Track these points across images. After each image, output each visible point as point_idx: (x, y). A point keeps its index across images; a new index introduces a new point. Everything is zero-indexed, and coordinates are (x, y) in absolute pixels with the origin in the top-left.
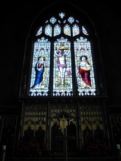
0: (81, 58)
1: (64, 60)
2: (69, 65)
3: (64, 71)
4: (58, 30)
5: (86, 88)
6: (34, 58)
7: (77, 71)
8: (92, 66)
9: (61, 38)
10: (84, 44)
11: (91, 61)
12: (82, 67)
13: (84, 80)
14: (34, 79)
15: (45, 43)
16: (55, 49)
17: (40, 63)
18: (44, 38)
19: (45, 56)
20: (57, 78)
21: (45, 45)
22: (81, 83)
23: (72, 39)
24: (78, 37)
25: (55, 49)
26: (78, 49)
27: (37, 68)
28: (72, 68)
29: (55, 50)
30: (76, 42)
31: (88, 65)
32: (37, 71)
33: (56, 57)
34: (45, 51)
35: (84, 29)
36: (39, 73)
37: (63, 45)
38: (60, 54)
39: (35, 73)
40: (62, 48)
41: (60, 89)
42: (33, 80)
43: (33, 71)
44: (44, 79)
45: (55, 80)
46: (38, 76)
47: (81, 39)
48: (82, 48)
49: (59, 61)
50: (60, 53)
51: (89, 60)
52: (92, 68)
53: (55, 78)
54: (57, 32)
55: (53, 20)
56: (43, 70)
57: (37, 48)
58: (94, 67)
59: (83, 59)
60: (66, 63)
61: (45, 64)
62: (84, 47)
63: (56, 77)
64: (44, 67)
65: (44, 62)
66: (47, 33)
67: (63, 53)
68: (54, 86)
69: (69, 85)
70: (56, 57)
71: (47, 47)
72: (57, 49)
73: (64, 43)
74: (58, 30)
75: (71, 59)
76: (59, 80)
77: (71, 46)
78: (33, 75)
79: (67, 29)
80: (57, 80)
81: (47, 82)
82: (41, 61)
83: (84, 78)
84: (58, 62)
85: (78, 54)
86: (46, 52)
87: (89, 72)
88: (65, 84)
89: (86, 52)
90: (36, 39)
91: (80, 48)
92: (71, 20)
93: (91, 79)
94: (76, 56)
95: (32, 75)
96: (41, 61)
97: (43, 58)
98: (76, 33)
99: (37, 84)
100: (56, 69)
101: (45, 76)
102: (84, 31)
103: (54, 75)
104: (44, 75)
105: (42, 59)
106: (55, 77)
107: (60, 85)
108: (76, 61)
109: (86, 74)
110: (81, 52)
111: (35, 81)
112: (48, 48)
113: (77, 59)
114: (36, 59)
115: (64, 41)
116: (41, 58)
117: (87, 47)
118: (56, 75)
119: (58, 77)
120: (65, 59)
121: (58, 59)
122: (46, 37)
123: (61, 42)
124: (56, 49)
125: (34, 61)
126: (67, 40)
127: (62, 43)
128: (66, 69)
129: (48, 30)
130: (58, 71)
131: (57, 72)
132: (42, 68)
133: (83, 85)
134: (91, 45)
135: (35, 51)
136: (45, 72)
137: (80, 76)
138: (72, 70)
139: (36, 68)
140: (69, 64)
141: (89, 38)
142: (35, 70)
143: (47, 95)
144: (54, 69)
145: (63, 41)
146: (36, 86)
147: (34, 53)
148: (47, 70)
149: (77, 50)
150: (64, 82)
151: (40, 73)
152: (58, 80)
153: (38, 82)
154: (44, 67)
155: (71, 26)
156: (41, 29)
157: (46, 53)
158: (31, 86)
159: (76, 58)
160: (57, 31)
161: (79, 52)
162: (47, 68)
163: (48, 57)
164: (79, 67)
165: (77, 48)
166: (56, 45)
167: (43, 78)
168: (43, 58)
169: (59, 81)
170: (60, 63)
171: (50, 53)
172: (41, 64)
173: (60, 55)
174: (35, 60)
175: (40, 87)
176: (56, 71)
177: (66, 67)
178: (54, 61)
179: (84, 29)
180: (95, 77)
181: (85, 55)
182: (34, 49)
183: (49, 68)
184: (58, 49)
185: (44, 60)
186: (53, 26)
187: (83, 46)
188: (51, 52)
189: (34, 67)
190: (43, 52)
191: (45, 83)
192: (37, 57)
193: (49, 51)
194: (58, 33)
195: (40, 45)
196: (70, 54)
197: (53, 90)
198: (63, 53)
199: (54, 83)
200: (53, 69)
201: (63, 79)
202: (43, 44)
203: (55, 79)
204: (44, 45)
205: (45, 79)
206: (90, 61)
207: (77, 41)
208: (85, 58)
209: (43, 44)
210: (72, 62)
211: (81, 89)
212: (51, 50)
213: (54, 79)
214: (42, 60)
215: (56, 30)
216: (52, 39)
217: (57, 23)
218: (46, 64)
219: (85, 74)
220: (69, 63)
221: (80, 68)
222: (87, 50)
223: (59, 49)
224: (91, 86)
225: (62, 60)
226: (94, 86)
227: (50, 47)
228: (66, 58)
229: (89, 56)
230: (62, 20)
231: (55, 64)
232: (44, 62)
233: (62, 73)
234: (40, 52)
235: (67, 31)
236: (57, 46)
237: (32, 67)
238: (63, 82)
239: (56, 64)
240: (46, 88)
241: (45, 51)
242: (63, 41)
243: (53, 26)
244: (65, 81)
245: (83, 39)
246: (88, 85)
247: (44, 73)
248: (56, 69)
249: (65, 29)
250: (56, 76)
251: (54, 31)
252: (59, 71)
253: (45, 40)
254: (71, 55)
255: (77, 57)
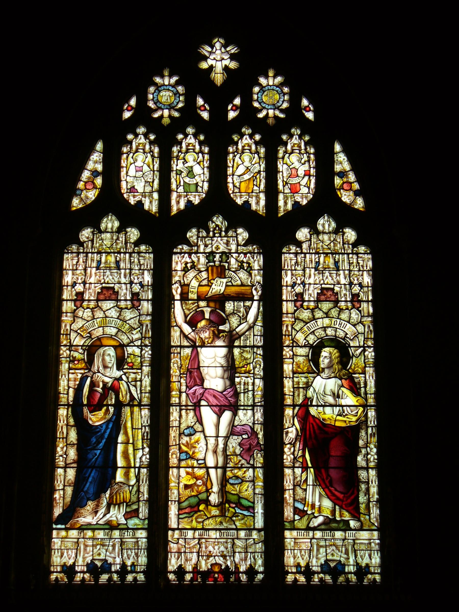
0: (316, 350)
1: (223, 362)
2: (250, 393)
3: (223, 431)
4: (192, 166)
5: (334, 525)
6: (64, 352)
7: (292, 431)
8: (371, 401)
9: (212, 225)
10: (336, 263)
11: (370, 371)
12: (321, 409)
13: (322, 481)
14: (71, 473)
15: (119, 253)
16: (177, 297)
17: (99, 377)
18: (117, 224)
19: (126, 341)
20: (190, 470)
21: (122, 265)
22: (309, 499)
23: (273, 233)
24: (305, 215)
25: (177, 297)
26: (300, 297)
27: (85, 410)
28: (265, 414)
29: (177, 304)
30: (296, 254)
31: (349, 399)
32: (81, 424)
33: (186, 343)
34: (122, 304)
35: (342, 162)
36: (94, 440)
37: (221, 272)
38: (203, 329)
39: (73, 436)
40: (219, 286)
41: (203, 529)
42: (65, 477)
43: (61, 423)
44: (119, 476)
45: (179, 479)
46: (90, 456)
47: (320, 228)
48: (322, 289)
49: (199, 367)
50: (203, 323)
51: (356, 363)
52: (372, 413)
53: (179, 467)
54: (187, 180)
55: (166, 94)
56: (116, 424)
57: (79, 288)
58: (379, 408)
59: (327, 361)
60: (237, 380)
61: (123, 386)
62: (332, 274)
63: (183, 464)
64: (119, 405)
65: (118, 374)
66: (132, 190)
67: (218, 320)
68: (173, 510)
69: (247, 508)
70: (181, 347)
71: (131, 283)
72: (191, 296)
73: (226, 255)
74: (197, 170)
75: (265, 357)
76: (197, 478)
77: (264, 277)
78: (66, 451)
79: (247, 164)
80: (186, 480)
81: (135, 489)
82: (105, 367)
83: (327, 469)
84: (195, 374)
85: (300, 334)
86: (128, 315)
87: (350, 434)
88: (229, 502)
89: (344, 316)
90: (66, 229)
91: (312, 293)
92: (271, 94)
93: (362, 474)
94: (287, 343)
95: (59, 449)
96: (105, 367)
97: (112, 352)
98: (294, 190)
99: (88, 499)
100: (180, 416)
101: (126, 455)
102: (342, 174)
103: (174, 450)
104: (120, 448)
105: (110, 354)
106: (180, 460)
107: (202, 507)
108: (287, 368)
109: (336, 449)
110: (318, 314)
111: (78, 484)
112: (142, 285)
113: (294, 359)
114: (76, 354)
115: (228, 243)
116: (101, 350)
117: (351, 284)
118: (184, 448)
119: (195, 464)
120: (233, 360)
121: (195, 357)
122: (131, 215)
123: (208, 250)
124: (184, 298)
125: (64, 367)
126: (243, 234)
127: (218, 256)
128: (235, 414)
129: (139, 164)
130: (192, 431)
131: (187, 432)
132: (112, 409)
133: (317, 507)
134: (375, 273)
135: (67, 306)
136: (126, 433)
137: (303, 456)
138: (266, 424)
139: (76, 407)
140: (250, 388)
141: (370, 229)
142: (72, 421)
143: (141, 577)
144: (174, 414)
145: (219, 244)
146: (82, 511)
147: (66, 319)
148: (138, 420)
149: (299, 304)
150: (223, 491)
151: (102, 436)
152: (192, 482)
153: (89, 487)
154: (119, 405)
155: (271, 139)
156: (95, 161)
157: (131, 322)
158: (57, 511)
159: (287, 352)
160: (190, 172)
161: (305, 315)
162: (136, 409)
163: (141, 347)
164: (300, 406)
165: (298, 289)
166: (185, 270)
167: (115, 468)
168: (115, 347)
169: (199, 482)
170: (202, 380)
171: (152, 321)
172: (105, 384)
173: (205, 335)
174: (72, 360)
175: (100, 518)
176: (183, 426)
177: (235, 408)
178: (175, 371)
179: (342, 162)
180: (379, 468)
181: (341, 334)
182: (65, 296)
183: (146, 412)
184: (193, 296)
185: (121, 363)
186: (165, 140)
187: (330, 280)
188: (153, 314)
189: (68, 405)
190: (113, 313)
191: (126, 493)
192: (78, 341)
193: (147, 307)
194: (197, 185)
195: (94, 264)
196: (258, 329)
197: (170, 533)
198: (223, 322)
199: (174, 495)
200: (168, 414)
201: (219, 471)
202: (112, 259)
203: (175, 470)
204: (118, 268)
205: (127, 475)
206: (364, 373)
207: (299, 244)
208: (335, 353)
209: (112, 259)
210: (264, 378)
211: (308, 529)
212: (154, 302)
213: (173, 473)
214: (107, 358)
215: (180, 166)
216: (163, 232)
217: (189, 115)
218: (133, 389)
219: (330, 449)
220: (253, 385)
221: (308, 412)
222: (352, 301)
223: (200, 298)
224: (356, 515)
225: (212, 358)
226: (375, 512)
227: (148, 278)
228: (236, 351)
229: (361, 338)
230: (218, 98)
231: (175, 386)
232: (118, 374)
233: (212, 441)
234: (99, 314)
235: (247, 177)
236: (191, 274)
237: (56, 404)
238: (215, 489)
239: (184, 388)
240: (133, 522)
241: (122, 304)
242: (219, 244)
243: (165, 140)
244: (229, 488)
245: (336, 232)
246: (341, 508)
247: (121, 438)
248: (180, 416)
249: (237, 158)
250: (183, 456)
251: (173, 174)
252: (198, 427)
253: (122, 237)
254: (265, 335)
255: (295, 344)
